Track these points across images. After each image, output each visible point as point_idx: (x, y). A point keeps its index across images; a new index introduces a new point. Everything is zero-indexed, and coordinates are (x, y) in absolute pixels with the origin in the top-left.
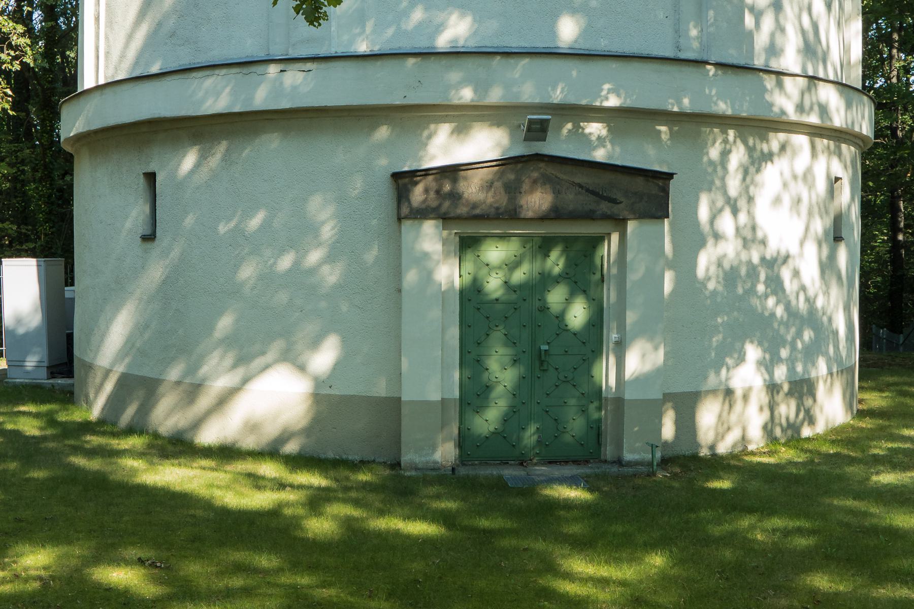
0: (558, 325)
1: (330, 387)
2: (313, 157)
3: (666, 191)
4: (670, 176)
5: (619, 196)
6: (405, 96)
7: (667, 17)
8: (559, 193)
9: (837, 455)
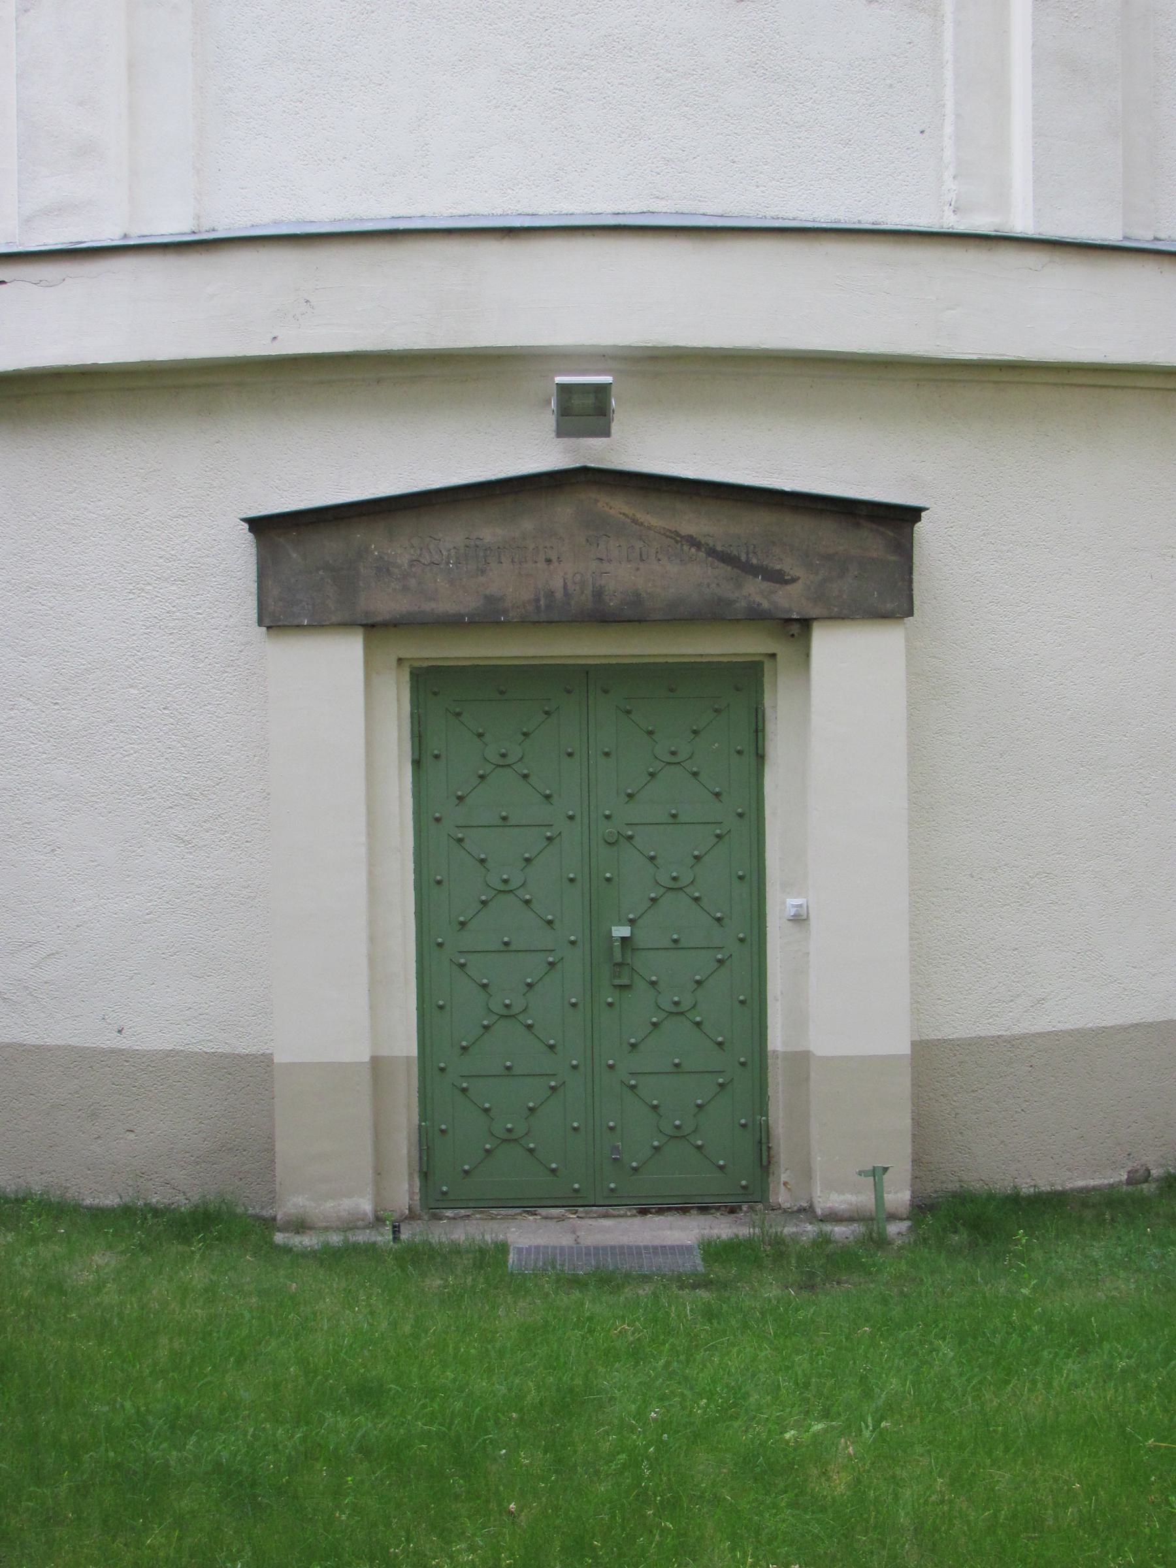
0: (655, 875)
1: (120, 1031)
2: (75, 485)
3: (904, 550)
4: (910, 515)
5: (788, 565)
6: (275, 338)
7: (922, 132)
8: (642, 560)
9: (714, 1252)
